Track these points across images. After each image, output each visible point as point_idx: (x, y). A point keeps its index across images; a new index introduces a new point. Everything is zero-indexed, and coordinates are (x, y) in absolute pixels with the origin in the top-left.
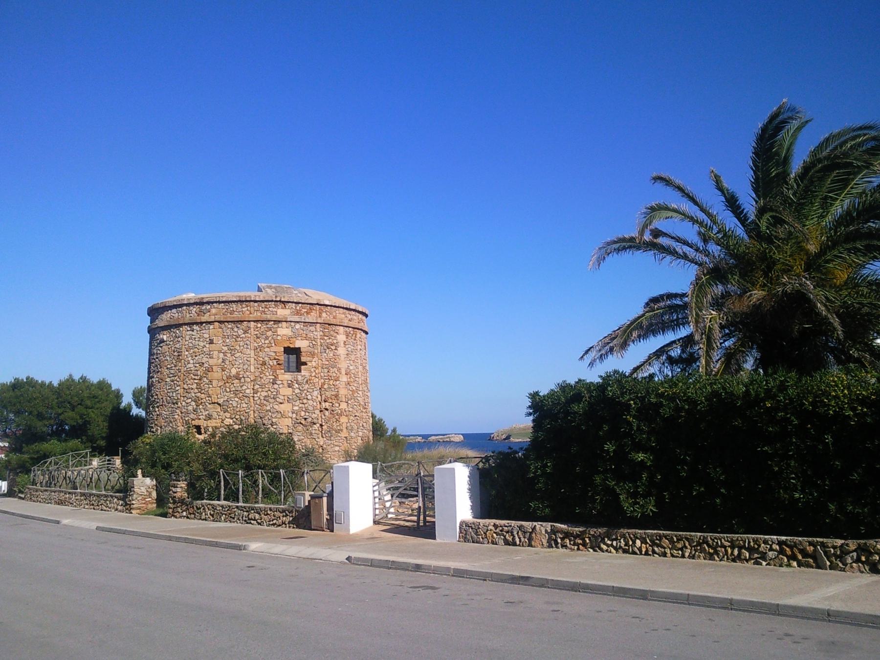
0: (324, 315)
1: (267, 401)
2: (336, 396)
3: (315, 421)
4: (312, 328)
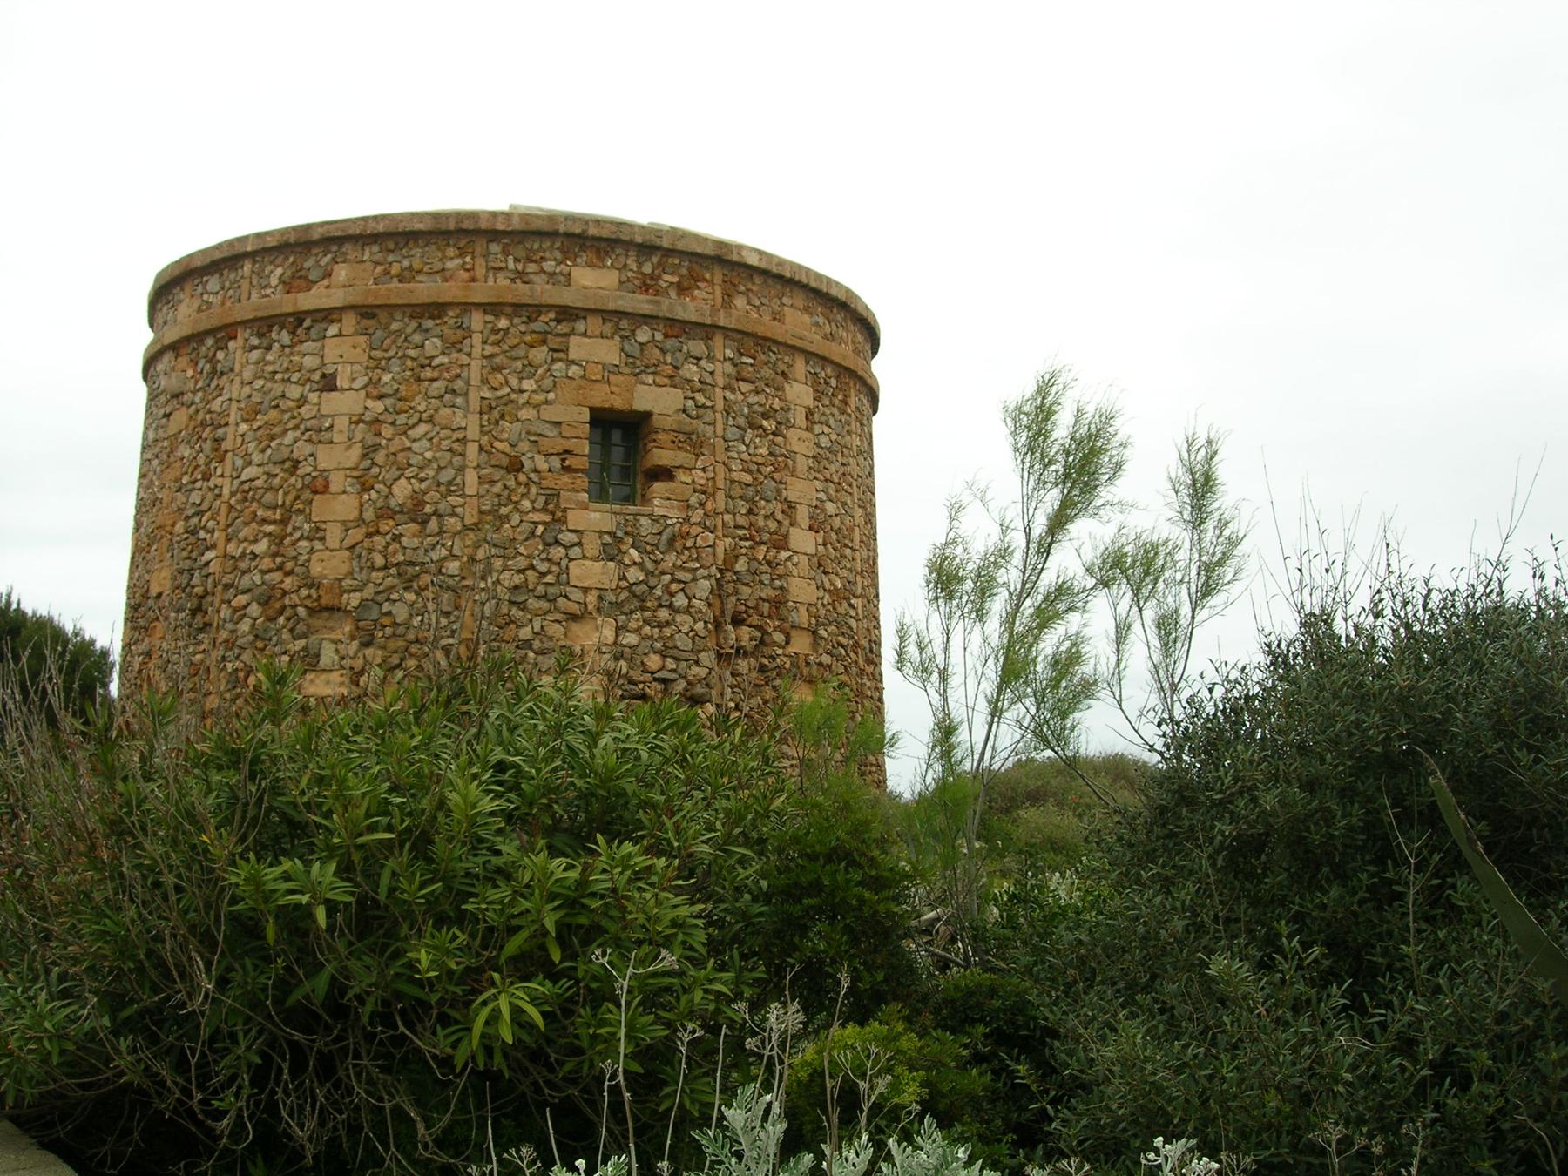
0: (740, 302)
1: (522, 606)
2: (778, 603)
3: (699, 690)
4: (697, 347)
